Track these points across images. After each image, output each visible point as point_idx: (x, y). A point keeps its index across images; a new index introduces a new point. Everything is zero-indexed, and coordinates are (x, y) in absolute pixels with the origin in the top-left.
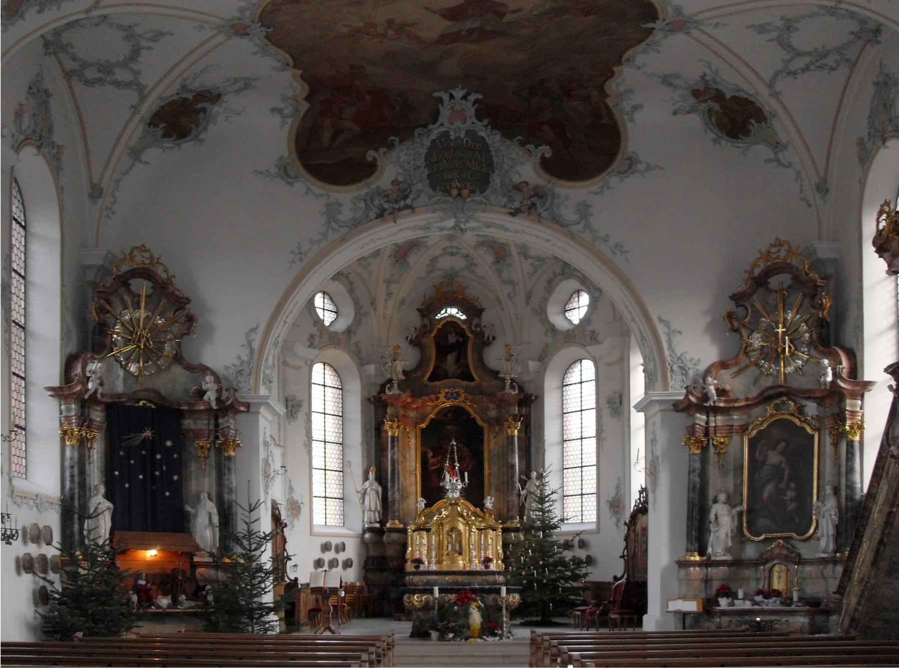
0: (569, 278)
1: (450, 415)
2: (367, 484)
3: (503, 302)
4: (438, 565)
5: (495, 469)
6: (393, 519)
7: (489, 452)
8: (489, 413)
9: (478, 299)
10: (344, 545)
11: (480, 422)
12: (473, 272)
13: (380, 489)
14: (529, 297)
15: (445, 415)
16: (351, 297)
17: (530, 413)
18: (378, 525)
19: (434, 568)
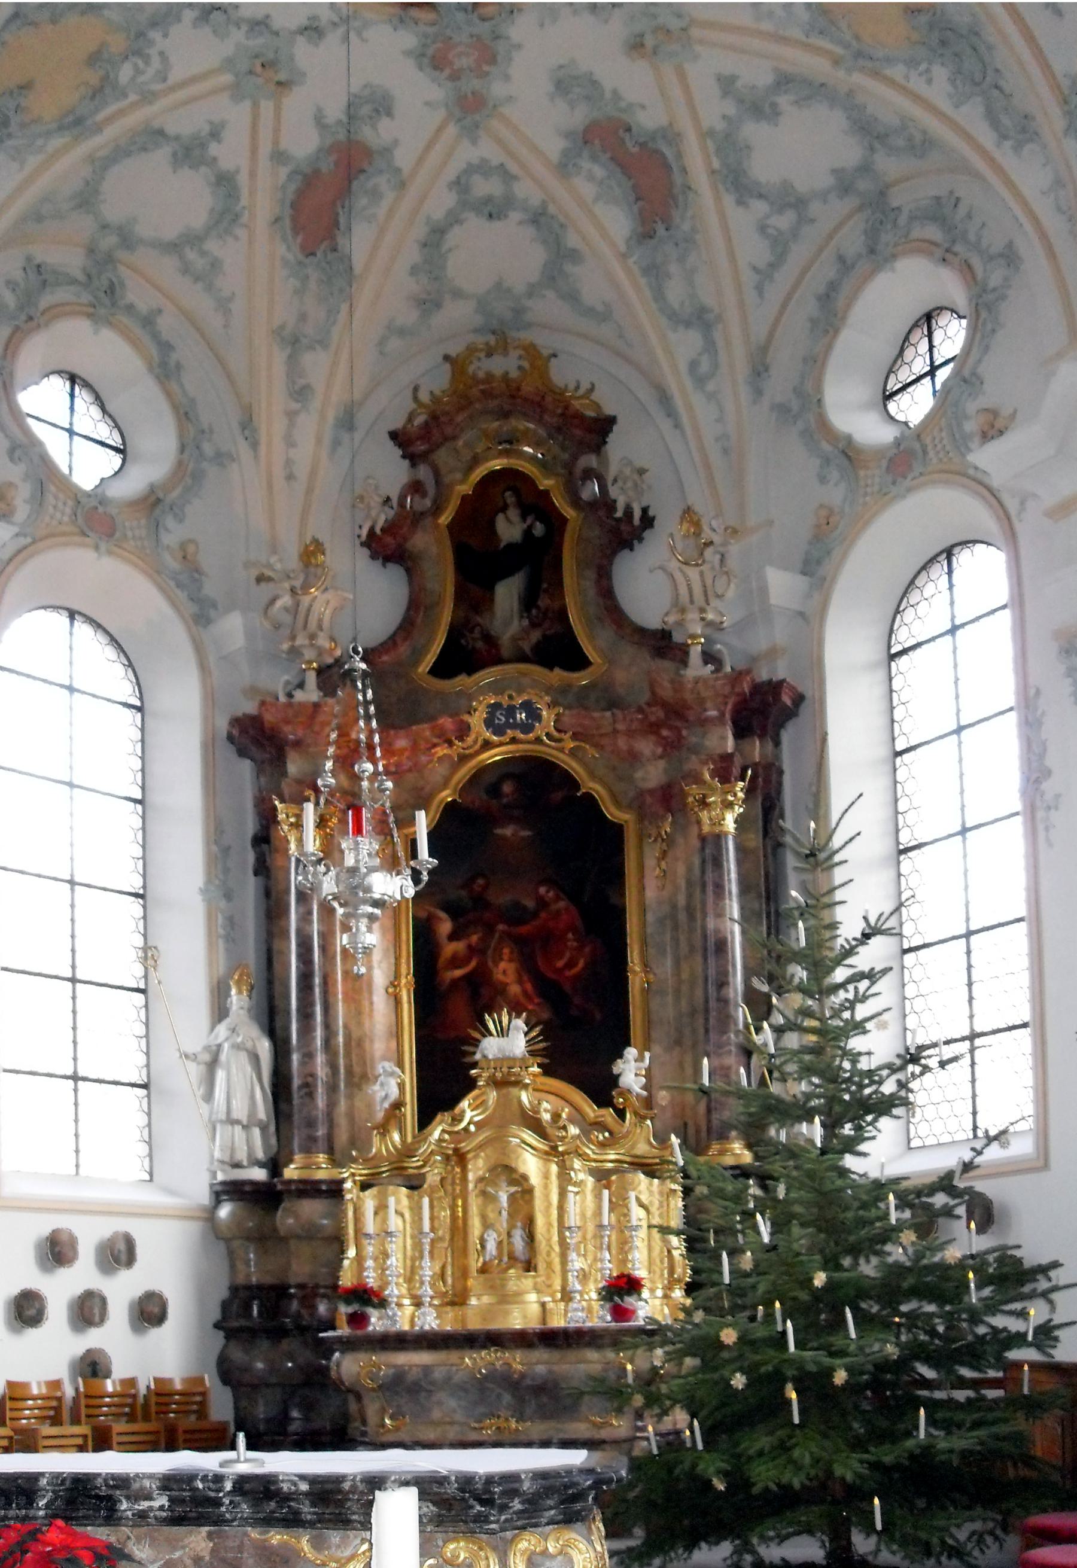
0: (894, 257)
1: (507, 788)
2: (222, 1029)
3: (679, 402)
4: (450, 1313)
5: (665, 968)
6: (308, 1148)
7: (643, 910)
8: (639, 775)
9: (592, 389)
10: (130, 1243)
11: (612, 813)
12: (572, 297)
13: (265, 1047)
14: (759, 370)
15: (494, 790)
16: (168, 394)
17: (778, 757)
18: (259, 1174)
19: (430, 1321)
